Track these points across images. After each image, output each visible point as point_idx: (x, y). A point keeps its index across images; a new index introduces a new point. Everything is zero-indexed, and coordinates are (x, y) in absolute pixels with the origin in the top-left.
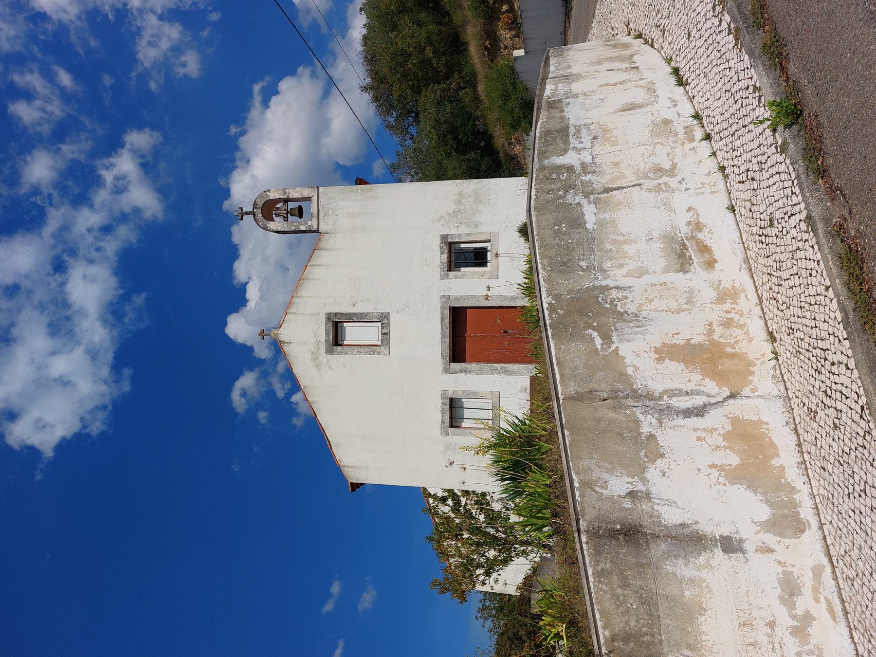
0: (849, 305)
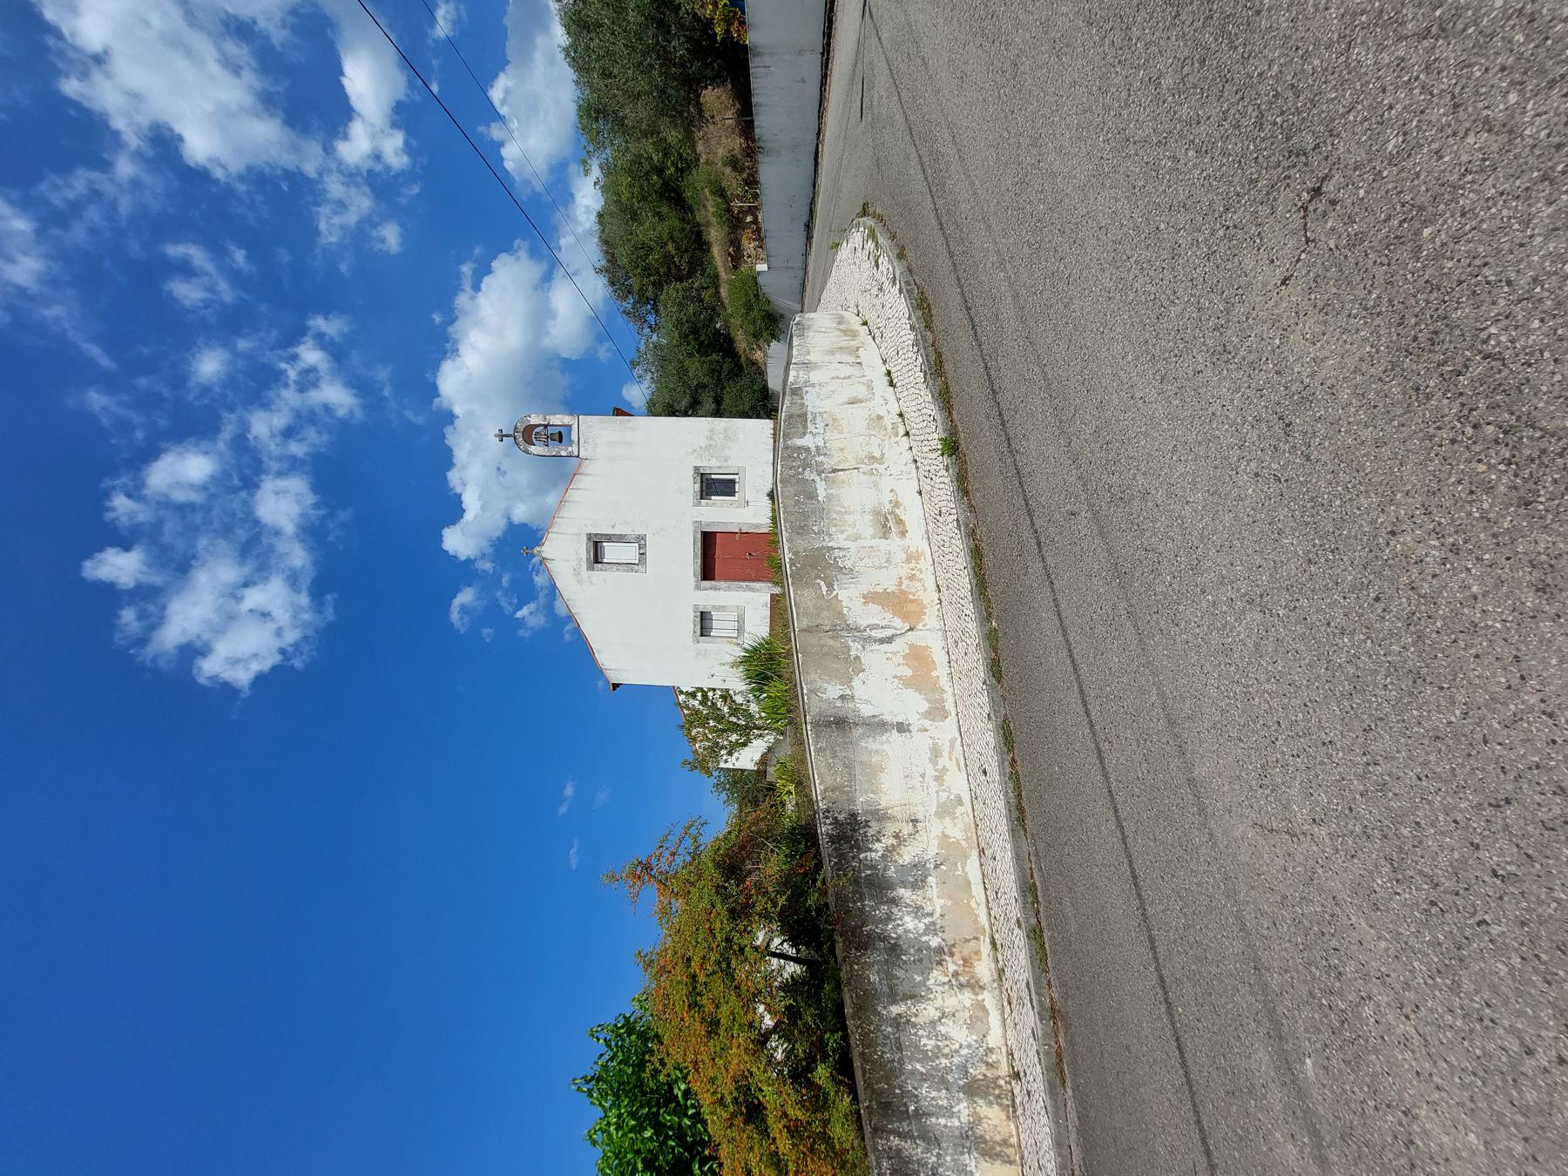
0: (974, 582)
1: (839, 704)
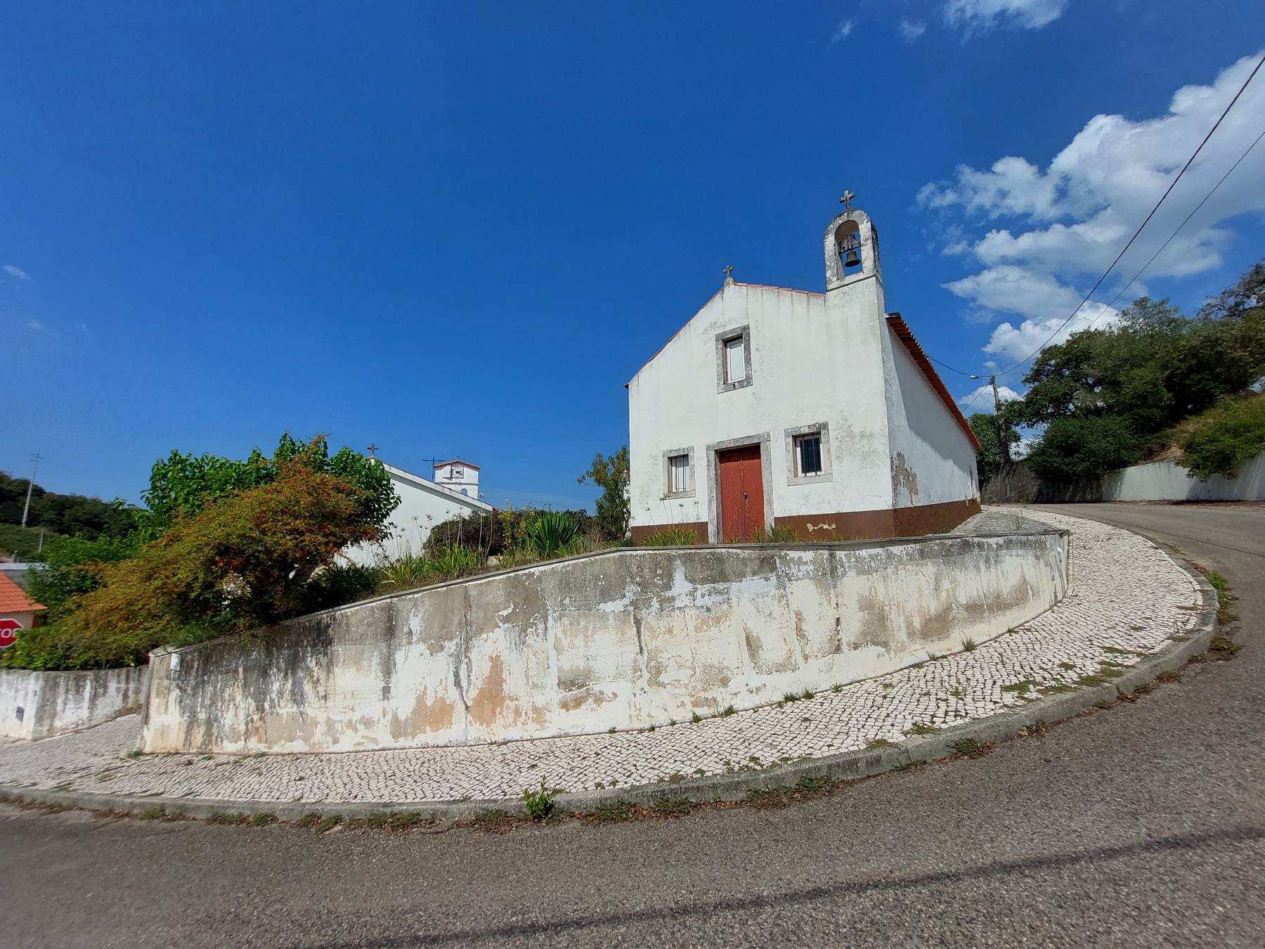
1: (406, 630)
